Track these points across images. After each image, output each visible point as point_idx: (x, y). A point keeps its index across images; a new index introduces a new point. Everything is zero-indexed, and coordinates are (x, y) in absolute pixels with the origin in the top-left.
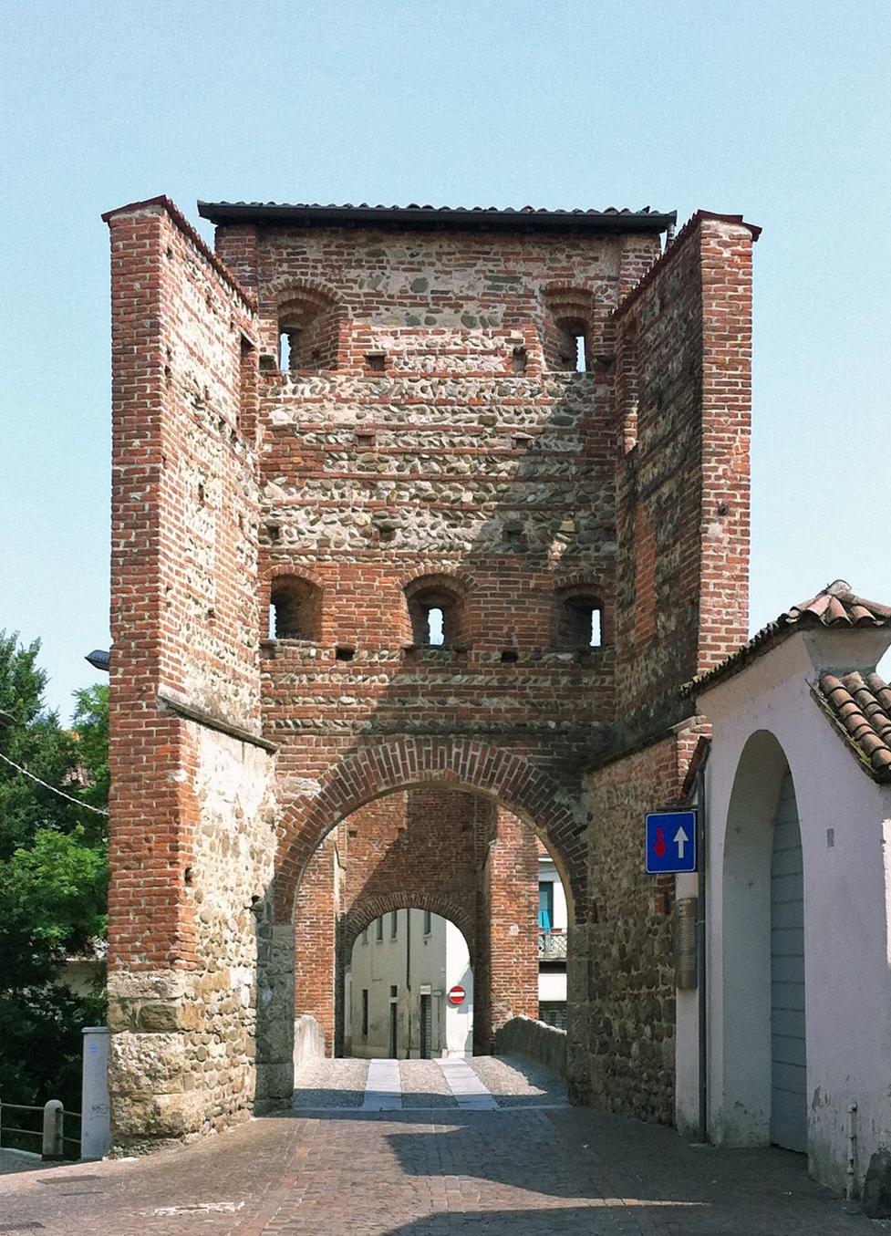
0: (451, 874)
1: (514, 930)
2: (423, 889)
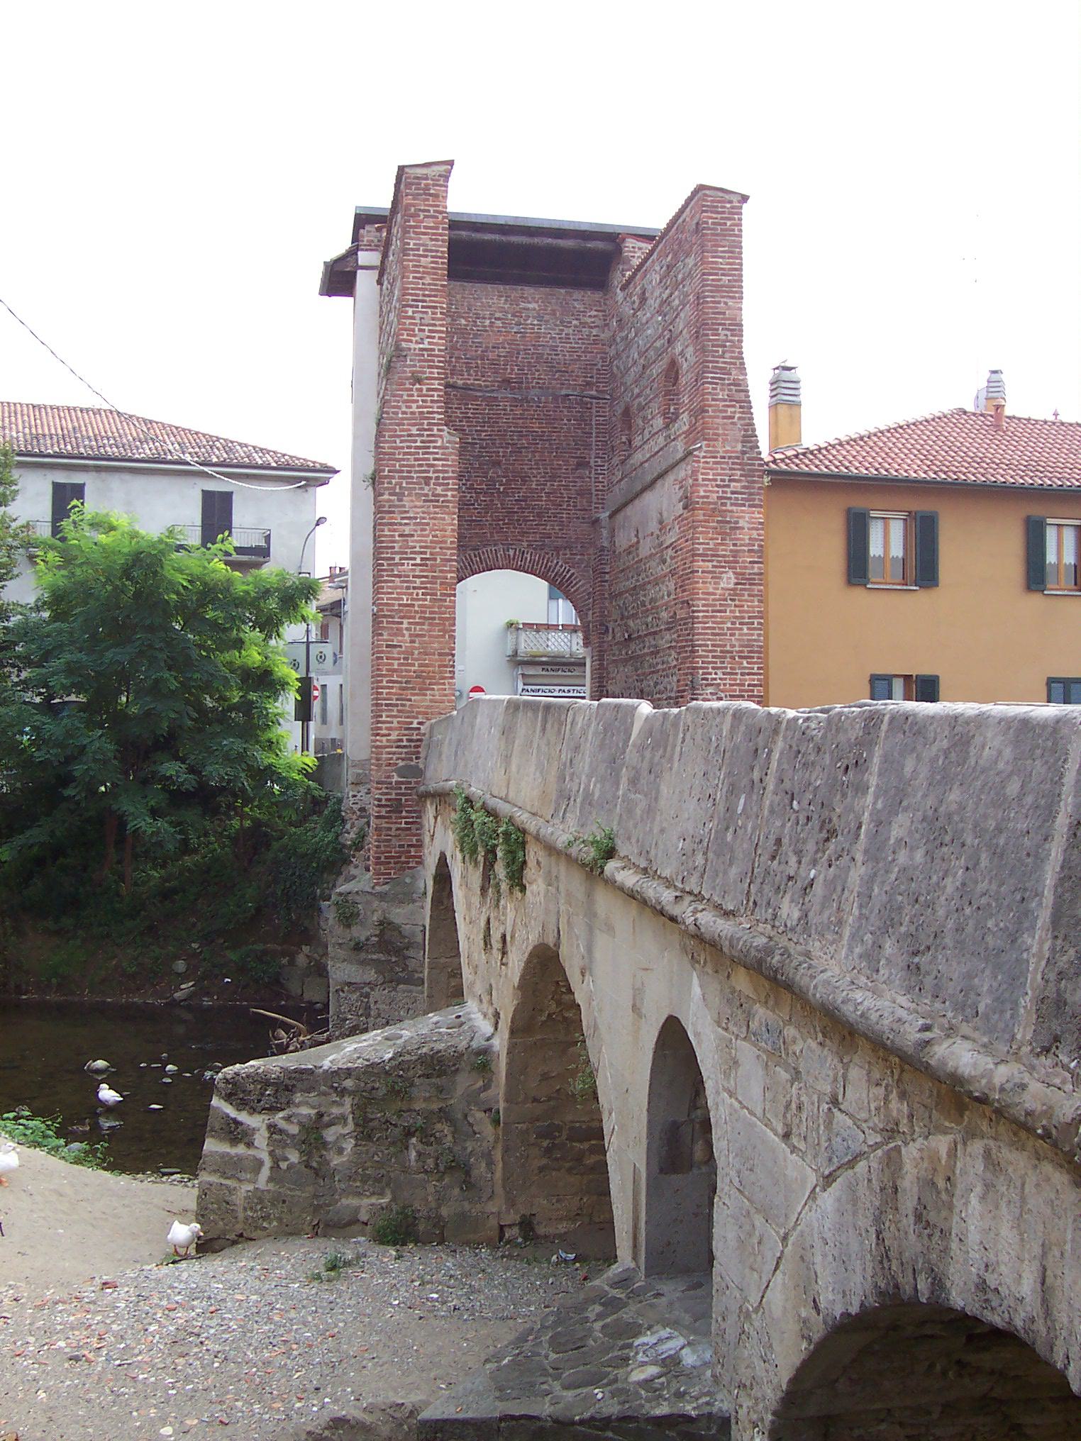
2: (525, 544)
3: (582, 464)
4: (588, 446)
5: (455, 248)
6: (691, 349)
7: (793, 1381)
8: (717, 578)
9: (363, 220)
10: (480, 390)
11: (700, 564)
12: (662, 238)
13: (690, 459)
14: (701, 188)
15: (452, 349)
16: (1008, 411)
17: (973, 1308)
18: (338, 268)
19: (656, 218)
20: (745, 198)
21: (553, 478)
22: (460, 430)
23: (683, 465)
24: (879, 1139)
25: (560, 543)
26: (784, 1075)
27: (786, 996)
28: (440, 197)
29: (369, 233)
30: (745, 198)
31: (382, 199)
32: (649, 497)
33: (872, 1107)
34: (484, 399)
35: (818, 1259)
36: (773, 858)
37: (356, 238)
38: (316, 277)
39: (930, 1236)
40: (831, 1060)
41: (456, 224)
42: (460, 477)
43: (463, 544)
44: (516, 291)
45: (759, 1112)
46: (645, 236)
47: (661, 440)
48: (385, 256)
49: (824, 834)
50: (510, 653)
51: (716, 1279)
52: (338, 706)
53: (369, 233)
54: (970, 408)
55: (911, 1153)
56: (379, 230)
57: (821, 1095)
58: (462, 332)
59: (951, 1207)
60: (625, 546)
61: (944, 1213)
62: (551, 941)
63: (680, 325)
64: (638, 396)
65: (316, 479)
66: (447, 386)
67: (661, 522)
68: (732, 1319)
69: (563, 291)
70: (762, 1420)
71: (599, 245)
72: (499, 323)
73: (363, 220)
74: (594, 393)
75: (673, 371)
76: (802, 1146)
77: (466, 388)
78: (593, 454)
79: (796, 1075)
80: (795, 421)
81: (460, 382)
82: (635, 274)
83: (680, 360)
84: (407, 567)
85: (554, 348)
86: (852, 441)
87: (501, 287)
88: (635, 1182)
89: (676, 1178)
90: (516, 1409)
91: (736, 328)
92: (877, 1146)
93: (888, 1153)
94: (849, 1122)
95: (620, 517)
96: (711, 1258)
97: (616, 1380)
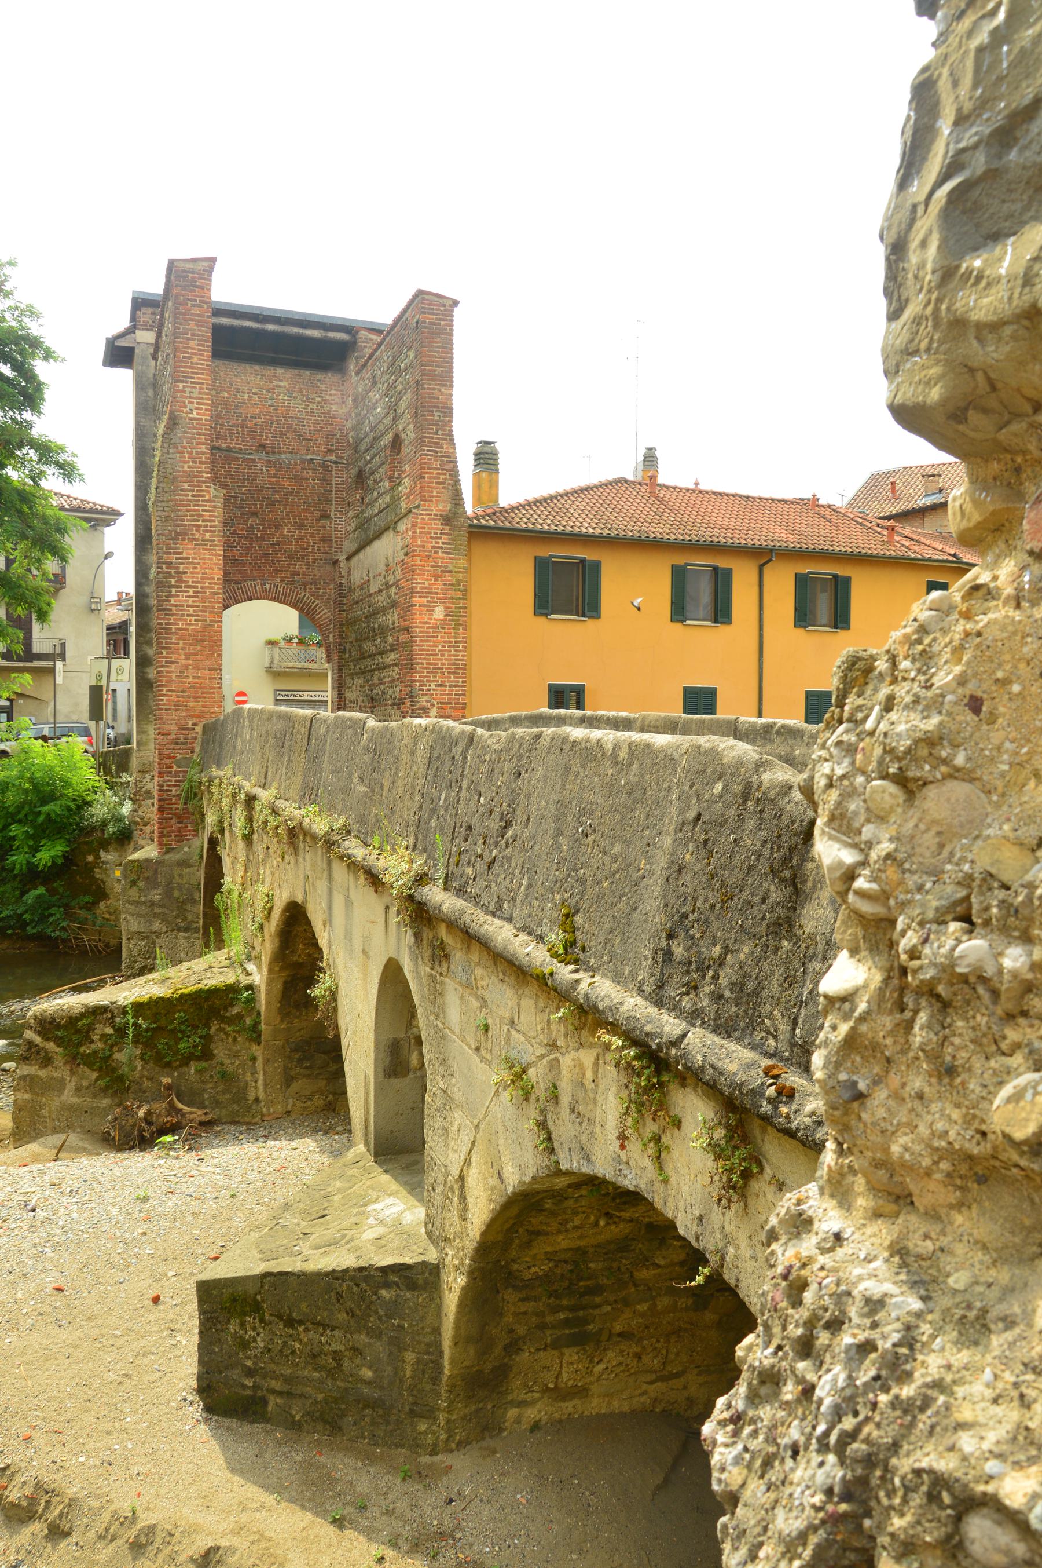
0: (308, 565)
1: (439, 613)
3: (325, 516)
4: (329, 501)
5: (218, 332)
6: (411, 426)
7: (484, 1234)
8: (431, 611)
9: (140, 303)
10: (240, 450)
11: (417, 600)
12: (389, 332)
13: (411, 515)
14: (420, 293)
15: (217, 417)
16: (661, 480)
17: (610, 1176)
18: (122, 343)
19: (384, 313)
20: (456, 303)
21: (301, 526)
22: (224, 486)
23: (405, 520)
24: (544, 1051)
25: (308, 579)
26: (475, 1004)
27: (475, 946)
28: (206, 287)
29: (145, 315)
30: (456, 303)
31: (156, 286)
32: (377, 545)
33: (539, 1027)
34: (245, 460)
35: (502, 1142)
36: (466, 840)
37: (133, 318)
38: (100, 351)
39: (581, 1123)
40: (509, 992)
41: (219, 311)
42: (225, 524)
43: (227, 580)
44: (269, 371)
45: (457, 1030)
46: (375, 329)
47: (387, 499)
48: (159, 336)
49: (503, 824)
50: (267, 665)
51: (427, 1159)
52: (126, 707)
53: (145, 315)
54: (630, 477)
55: (566, 1061)
56: (153, 313)
57: (502, 1018)
58: (225, 403)
59: (595, 1101)
60: (358, 583)
61: (590, 1107)
62: (299, 899)
63: (403, 405)
64: (370, 462)
65: (104, 520)
66: (214, 448)
67: (387, 565)
68: (439, 1189)
69: (308, 373)
70: (462, 1264)
71: (316, 333)
72: (256, 397)
73: (140, 303)
74: (333, 458)
75: (396, 443)
76: (488, 1057)
77: (229, 450)
78: (333, 508)
79: (484, 1003)
80: (494, 485)
81: (224, 446)
82: (367, 361)
83: (403, 436)
84: (182, 596)
85: (301, 420)
86: (537, 502)
87: (257, 367)
88: (367, 1086)
89: (395, 1081)
90: (274, 1267)
91: (448, 411)
92: (543, 1056)
93: (550, 1063)
94: (522, 1039)
95: (355, 560)
96: (424, 1143)
97: (352, 1240)
